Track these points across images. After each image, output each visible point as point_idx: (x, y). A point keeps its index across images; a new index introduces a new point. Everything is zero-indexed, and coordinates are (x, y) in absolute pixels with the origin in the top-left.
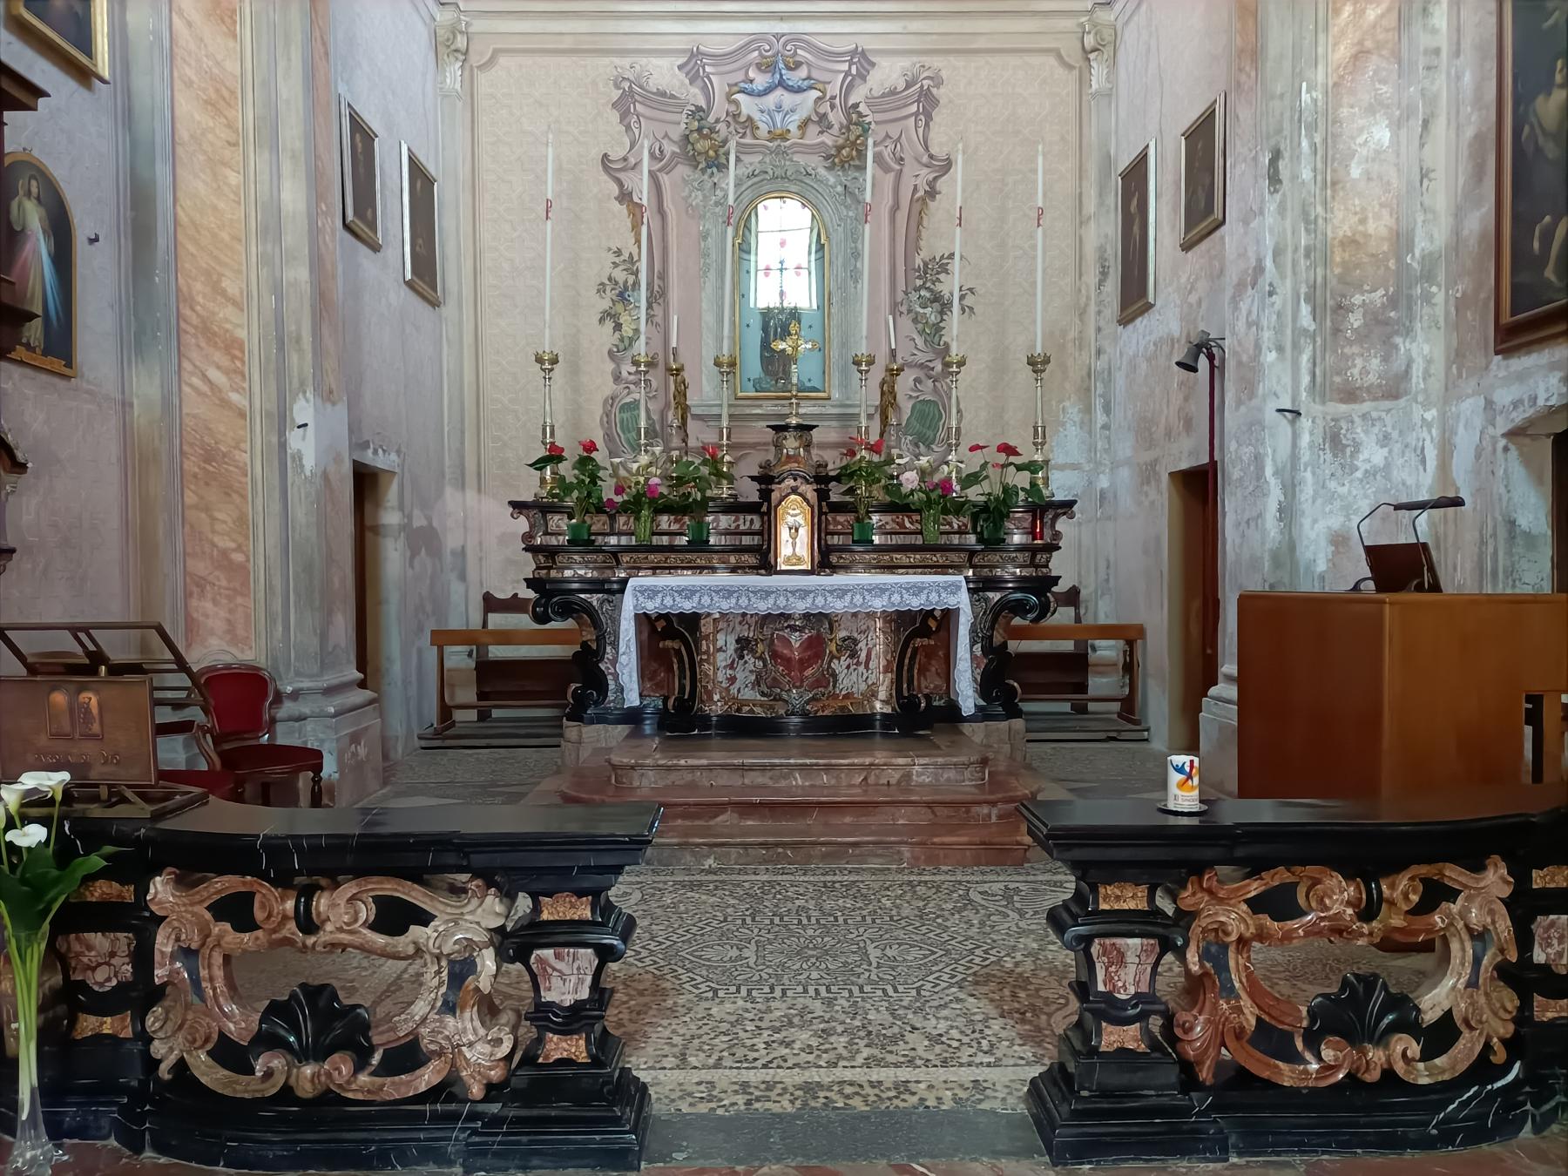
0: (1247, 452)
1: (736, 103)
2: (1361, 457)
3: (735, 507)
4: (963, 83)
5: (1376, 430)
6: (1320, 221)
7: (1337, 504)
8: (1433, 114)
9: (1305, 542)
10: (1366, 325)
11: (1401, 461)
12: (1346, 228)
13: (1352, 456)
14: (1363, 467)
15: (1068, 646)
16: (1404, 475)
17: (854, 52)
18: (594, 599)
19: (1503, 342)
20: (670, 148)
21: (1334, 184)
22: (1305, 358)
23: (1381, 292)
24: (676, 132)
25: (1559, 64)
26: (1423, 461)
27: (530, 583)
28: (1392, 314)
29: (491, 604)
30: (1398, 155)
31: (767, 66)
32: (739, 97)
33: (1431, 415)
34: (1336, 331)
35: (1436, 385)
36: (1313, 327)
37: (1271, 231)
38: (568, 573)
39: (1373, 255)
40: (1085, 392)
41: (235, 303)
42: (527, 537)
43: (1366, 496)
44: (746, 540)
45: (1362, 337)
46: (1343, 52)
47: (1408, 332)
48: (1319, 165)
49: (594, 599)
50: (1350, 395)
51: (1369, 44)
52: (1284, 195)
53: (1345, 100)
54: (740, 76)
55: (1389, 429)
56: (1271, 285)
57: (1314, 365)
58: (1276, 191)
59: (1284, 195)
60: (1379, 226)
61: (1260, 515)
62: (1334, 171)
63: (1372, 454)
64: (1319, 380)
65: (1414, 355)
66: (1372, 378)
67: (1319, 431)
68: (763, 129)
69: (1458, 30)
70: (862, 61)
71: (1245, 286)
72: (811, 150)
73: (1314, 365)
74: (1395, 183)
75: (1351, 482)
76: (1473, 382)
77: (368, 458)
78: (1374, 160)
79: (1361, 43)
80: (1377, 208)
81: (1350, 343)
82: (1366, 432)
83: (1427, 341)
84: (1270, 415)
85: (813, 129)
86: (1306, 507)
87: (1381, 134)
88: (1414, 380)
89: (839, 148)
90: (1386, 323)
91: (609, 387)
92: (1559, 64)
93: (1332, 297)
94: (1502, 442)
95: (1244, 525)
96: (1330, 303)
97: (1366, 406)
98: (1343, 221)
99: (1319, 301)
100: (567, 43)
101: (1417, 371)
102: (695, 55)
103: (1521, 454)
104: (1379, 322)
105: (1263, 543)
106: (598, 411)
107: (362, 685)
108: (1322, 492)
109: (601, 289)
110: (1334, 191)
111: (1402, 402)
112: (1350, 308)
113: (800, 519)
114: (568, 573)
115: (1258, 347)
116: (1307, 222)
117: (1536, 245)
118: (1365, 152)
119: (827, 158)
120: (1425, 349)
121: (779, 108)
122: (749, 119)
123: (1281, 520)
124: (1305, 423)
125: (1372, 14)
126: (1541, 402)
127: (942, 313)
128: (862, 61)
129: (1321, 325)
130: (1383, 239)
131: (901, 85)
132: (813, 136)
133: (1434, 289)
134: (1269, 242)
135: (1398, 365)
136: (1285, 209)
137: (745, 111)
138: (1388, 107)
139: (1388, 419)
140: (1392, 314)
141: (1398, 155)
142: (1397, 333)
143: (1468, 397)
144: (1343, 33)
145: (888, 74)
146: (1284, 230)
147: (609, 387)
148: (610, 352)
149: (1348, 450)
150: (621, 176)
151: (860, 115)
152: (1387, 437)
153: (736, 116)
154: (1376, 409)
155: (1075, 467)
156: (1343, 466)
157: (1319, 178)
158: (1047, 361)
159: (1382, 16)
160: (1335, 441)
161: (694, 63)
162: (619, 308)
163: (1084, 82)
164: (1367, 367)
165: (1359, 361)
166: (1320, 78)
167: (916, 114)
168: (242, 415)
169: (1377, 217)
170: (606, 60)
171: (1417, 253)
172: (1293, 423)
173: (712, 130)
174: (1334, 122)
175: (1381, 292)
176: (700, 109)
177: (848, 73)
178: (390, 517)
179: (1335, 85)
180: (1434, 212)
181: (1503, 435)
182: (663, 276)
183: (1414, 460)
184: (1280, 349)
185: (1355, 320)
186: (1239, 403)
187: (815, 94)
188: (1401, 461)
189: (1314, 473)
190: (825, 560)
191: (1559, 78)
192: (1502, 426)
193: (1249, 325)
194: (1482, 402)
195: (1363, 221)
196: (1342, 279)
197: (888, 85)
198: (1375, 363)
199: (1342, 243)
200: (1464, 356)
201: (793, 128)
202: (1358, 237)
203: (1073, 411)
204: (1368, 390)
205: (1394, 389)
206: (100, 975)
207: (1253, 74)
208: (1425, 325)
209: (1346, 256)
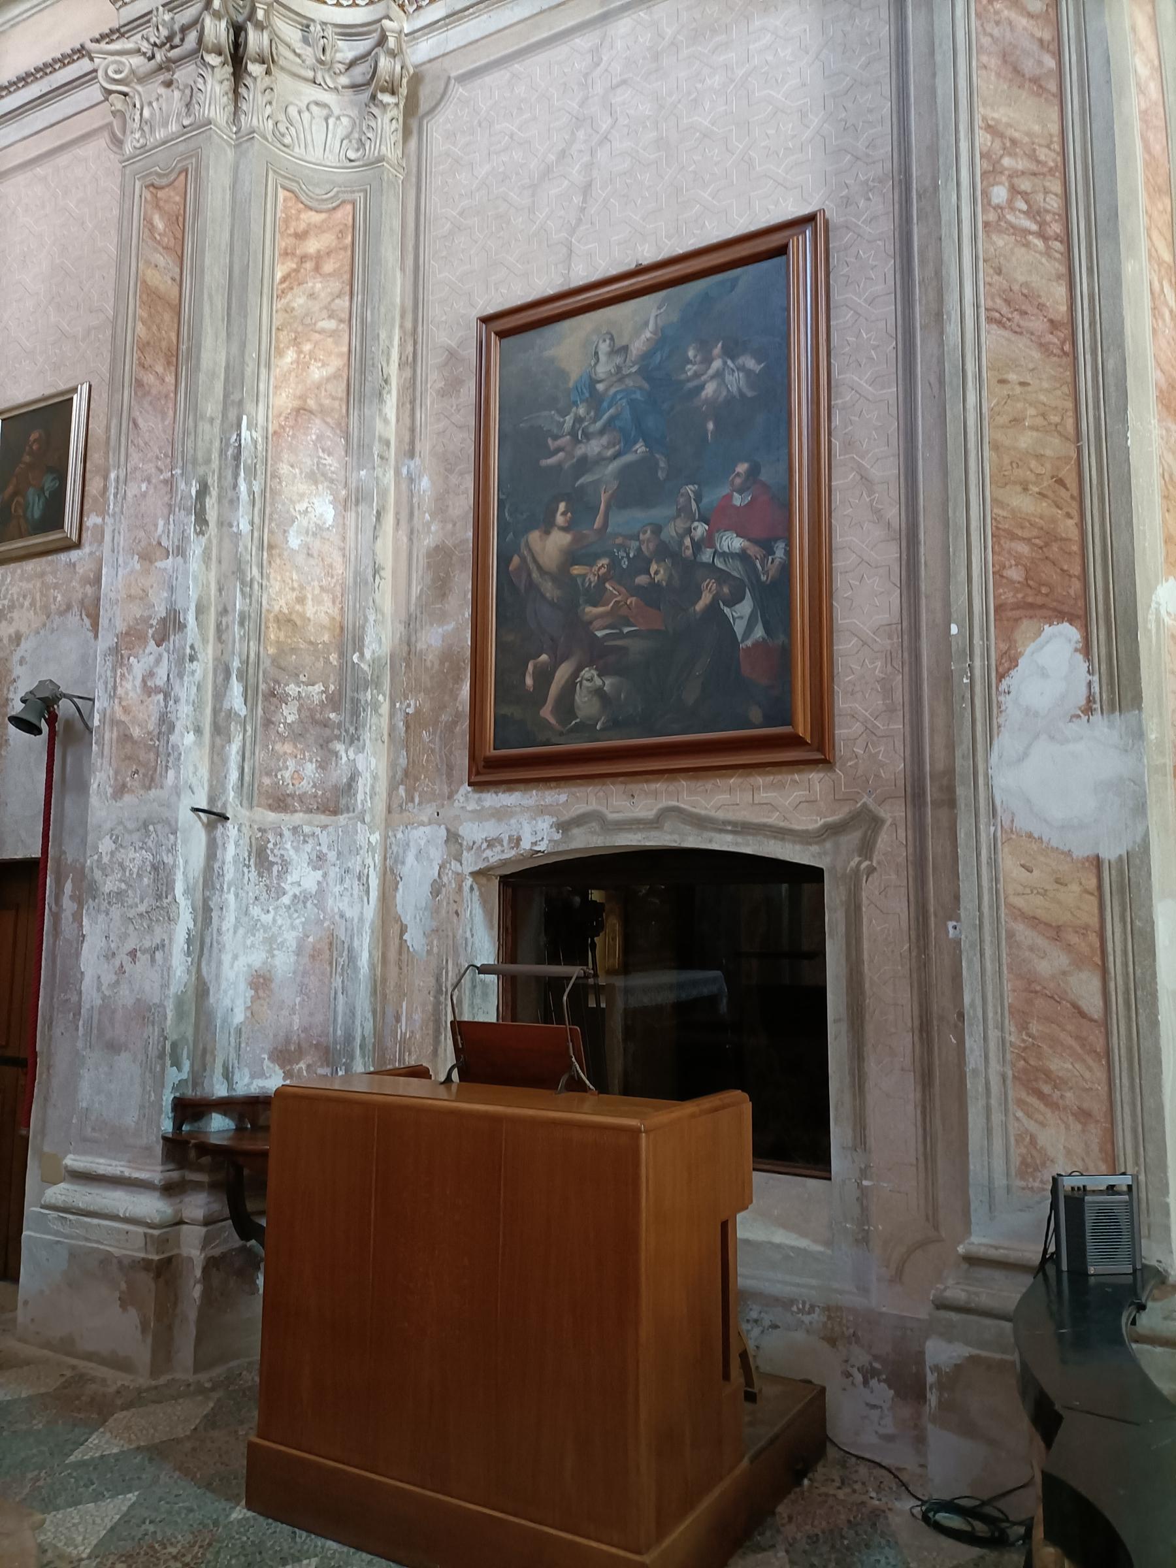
0: (135, 858)
2: (290, 879)
5: (308, 848)
6: (256, 586)
7: (260, 935)
8: (384, 507)
9: (224, 985)
10: (301, 721)
11: (337, 889)
12: (282, 602)
13: (279, 877)
14: (291, 890)
16: (343, 905)
19: (478, 773)
21: (271, 547)
22: (234, 748)
23: (319, 687)
25: (562, 506)
26: (368, 892)
28: (332, 716)
30: (344, 539)
33: (375, 838)
34: (268, 723)
35: (381, 806)
36: (243, 712)
37: (195, 578)
39: (311, 643)
43: (293, 928)
45: (297, 735)
46: (284, 400)
47: (353, 740)
48: (257, 520)
50: (280, 802)
51: (311, 403)
52: (209, 540)
53: (285, 456)
55: (325, 850)
56: (192, 647)
57: (243, 760)
58: (202, 533)
59: (209, 540)
60: (320, 612)
61: (161, 946)
62: (271, 532)
63: (303, 877)
64: (247, 778)
65: (361, 766)
66: (305, 786)
67: (244, 842)
69: (412, 430)
71: (142, 638)
73: (243, 760)
74: (339, 569)
75: (276, 908)
76: (430, 810)
78: (314, 534)
79: (303, 398)
80: (317, 591)
81: (284, 740)
82: (297, 850)
83: (374, 754)
84: (184, 815)
86: (227, 938)
87: (324, 509)
88: (360, 797)
90: (325, 724)
92: (562, 506)
93: (265, 681)
94: (469, 881)
95: (123, 957)
96: (262, 686)
97: (298, 818)
98: (279, 593)
99: (251, 681)
101: (363, 786)
103: (481, 894)
104: (315, 722)
105: (165, 986)
108: (245, 919)
110: (270, 555)
111: (342, 819)
112: (293, 698)
115: (166, 724)
116: (243, 583)
117: (529, 681)
118: (305, 523)
120: (370, 762)
123: (189, 954)
124: (231, 829)
125: (317, 373)
126: (526, 845)
129: (252, 710)
130: (323, 627)
133: (381, 698)
134: (193, 594)
135: (338, 775)
136: (209, 558)
138: (332, 481)
139: (324, 838)
140: (332, 716)
141: (344, 539)
142: (338, 738)
143: (422, 824)
144: (285, 378)
146: (209, 583)
149: (275, 869)
152: (321, 857)
154: (310, 823)
156: (268, 888)
157: (256, 534)
159: (328, 379)
160: (261, 857)
164: (301, 772)
165: (291, 763)
169: (318, 601)
171: (368, 655)
172: (210, 827)
174: (273, 476)
175: (319, 687)
179: (275, 433)
180: (383, 614)
181: (472, 874)
183: (357, 889)
184: (198, 731)
185: (290, 713)
186: (121, 790)
188: (337, 889)
189: (237, 895)
191: (560, 520)
192: (470, 863)
193: (149, 691)
194: (443, 832)
195: (301, 600)
196: (274, 661)
198: (310, 768)
199: (277, 620)
200: (417, 779)
202: (294, 617)
204: (301, 799)
205: (335, 801)
207: (170, 379)
208: (374, 736)
209: (282, 635)
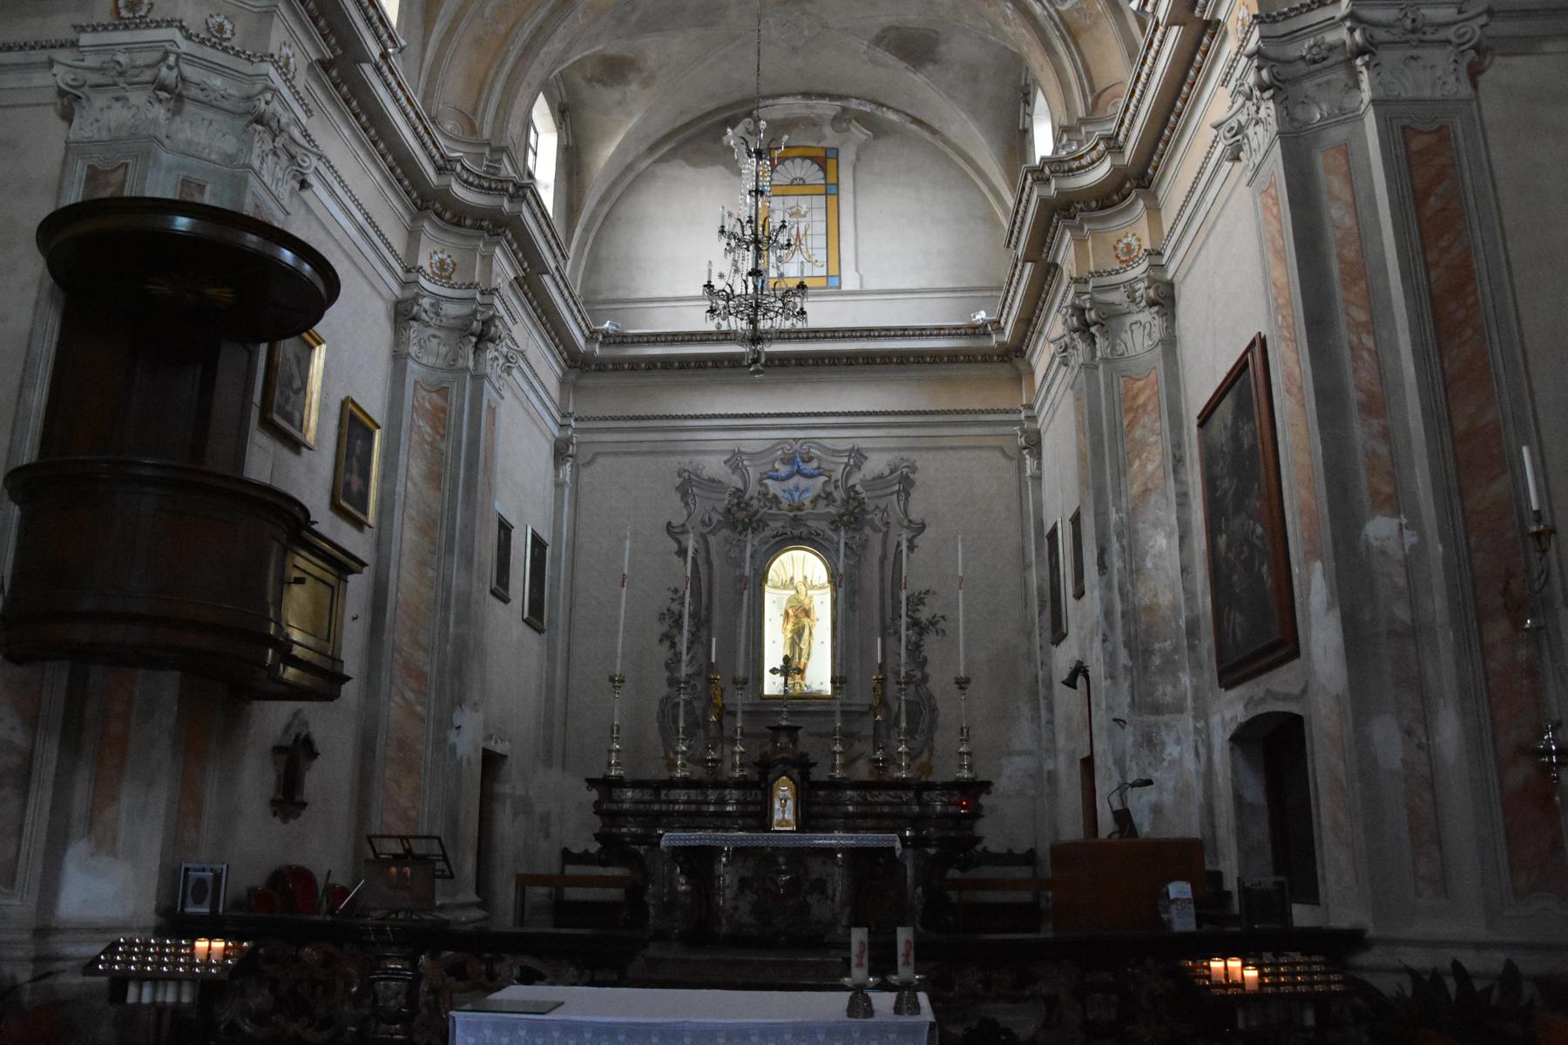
1: (766, 486)
3: (741, 784)
4: (929, 467)
15: (1025, 896)
17: (852, 450)
18: (642, 849)
20: (716, 518)
24: (721, 507)
27: (597, 837)
29: (567, 857)
31: (788, 460)
32: (768, 482)
34: (1146, 668)
38: (624, 830)
40: (1034, 695)
41: (425, 650)
42: (597, 804)
44: (751, 808)
49: (642, 849)
54: (769, 467)
68: (785, 504)
70: (858, 456)
72: (819, 517)
77: (492, 746)
85: (822, 503)
89: (841, 516)
91: (664, 690)
97: (1167, 717)
100: (646, 447)
102: (737, 454)
106: (655, 707)
107: (479, 906)
109: (662, 617)
113: (788, 794)
114: (624, 830)
119: (832, 523)
121: (797, 488)
122: (775, 496)
127: (920, 634)
128: (858, 456)
131: (887, 472)
132: (822, 508)
137: (772, 491)
145: (876, 464)
147: (664, 690)
148: (667, 664)
150: (680, 537)
151: (857, 493)
153: (765, 495)
155: (1029, 753)
158: (967, 681)
161: (735, 460)
162: (675, 631)
163: (1021, 468)
166: (1124, 505)
167: (898, 492)
168: (422, 720)
170: (673, 458)
173: (747, 504)
176: (738, 490)
177: (847, 464)
178: (504, 788)
182: (709, 608)
185: (1157, 660)
187: (824, 479)
190: (806, 821)
197: (876, 472)
201: (807, 503)
203: (1025, 709)
206: (392, 1003)
